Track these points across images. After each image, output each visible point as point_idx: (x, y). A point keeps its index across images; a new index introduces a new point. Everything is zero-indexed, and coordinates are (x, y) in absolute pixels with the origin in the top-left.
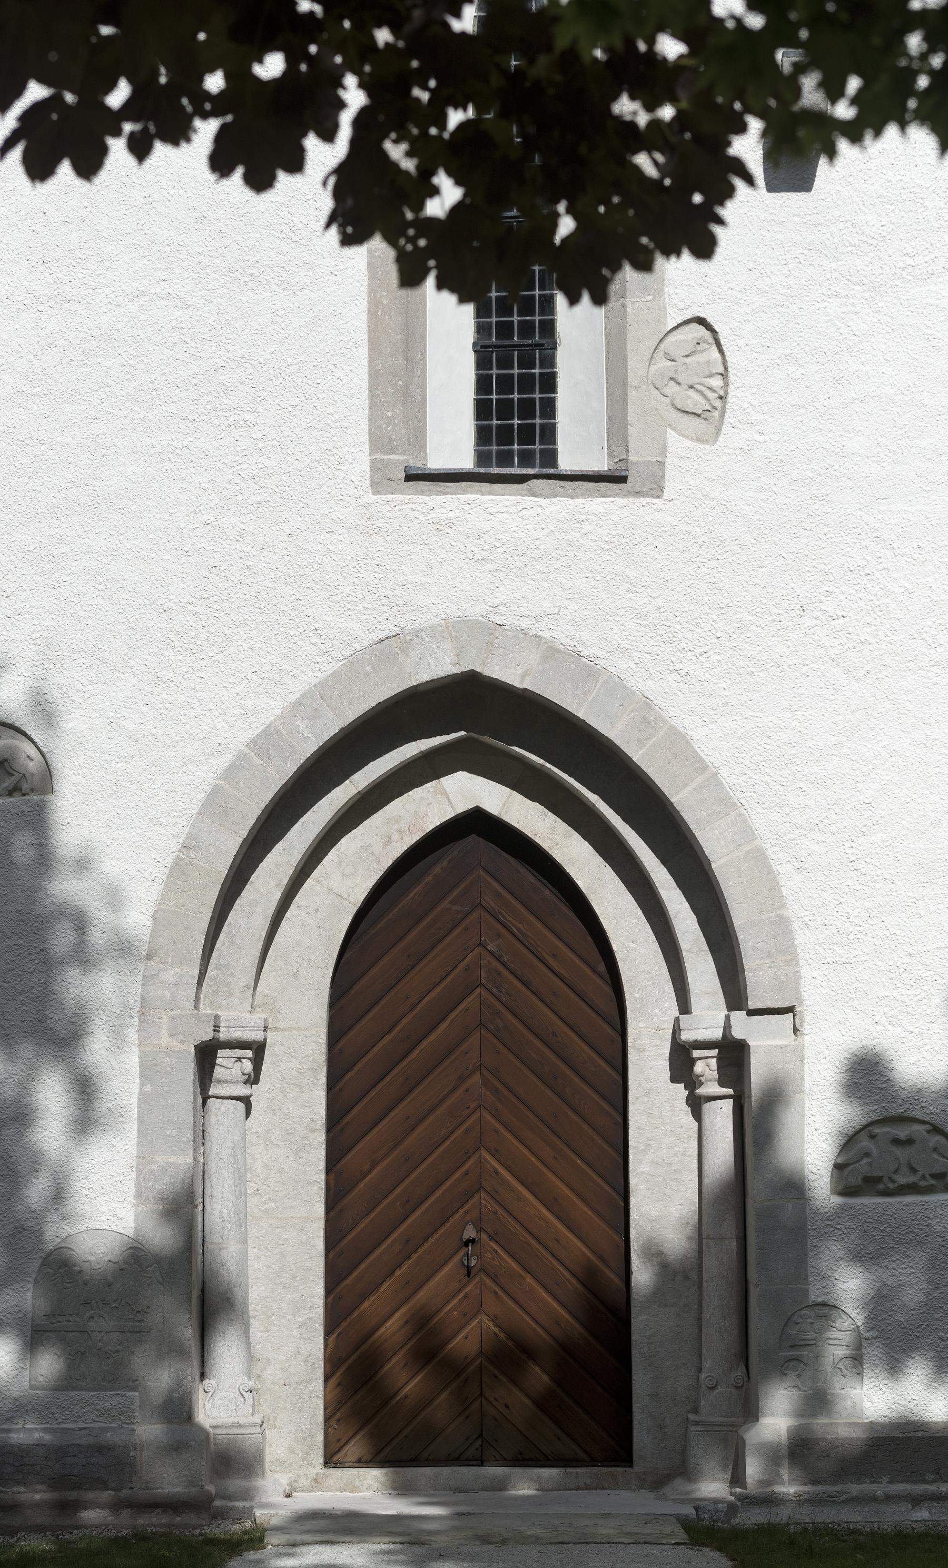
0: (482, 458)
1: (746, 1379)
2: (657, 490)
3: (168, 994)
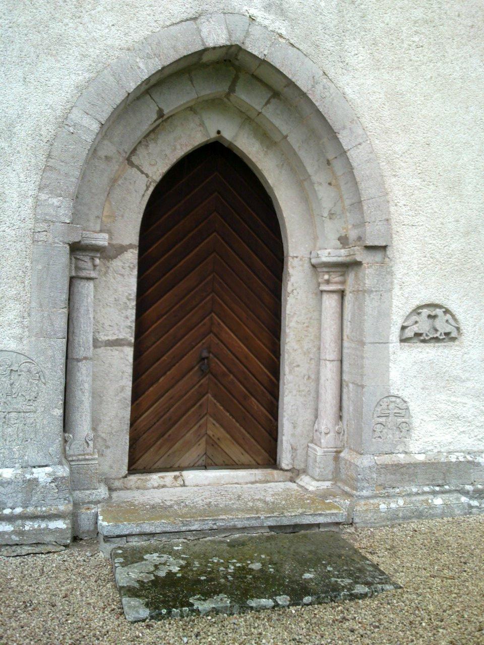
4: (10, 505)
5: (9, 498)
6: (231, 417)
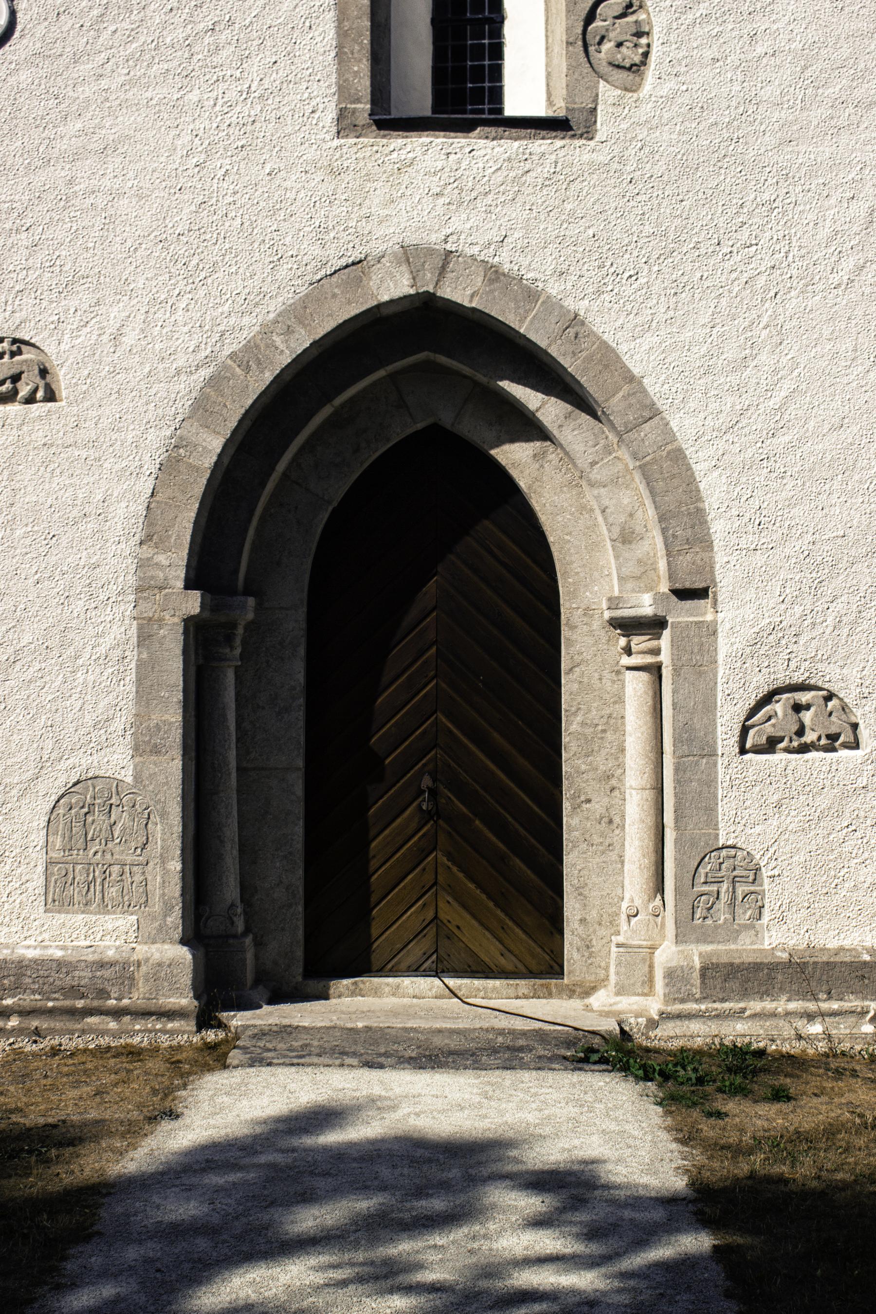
0: (437, 106)
1: (662, 909)
2: (588, 133)
3: (161, 575)
4: (116, 995)
5: (113, 984)
6: (478, 892)
